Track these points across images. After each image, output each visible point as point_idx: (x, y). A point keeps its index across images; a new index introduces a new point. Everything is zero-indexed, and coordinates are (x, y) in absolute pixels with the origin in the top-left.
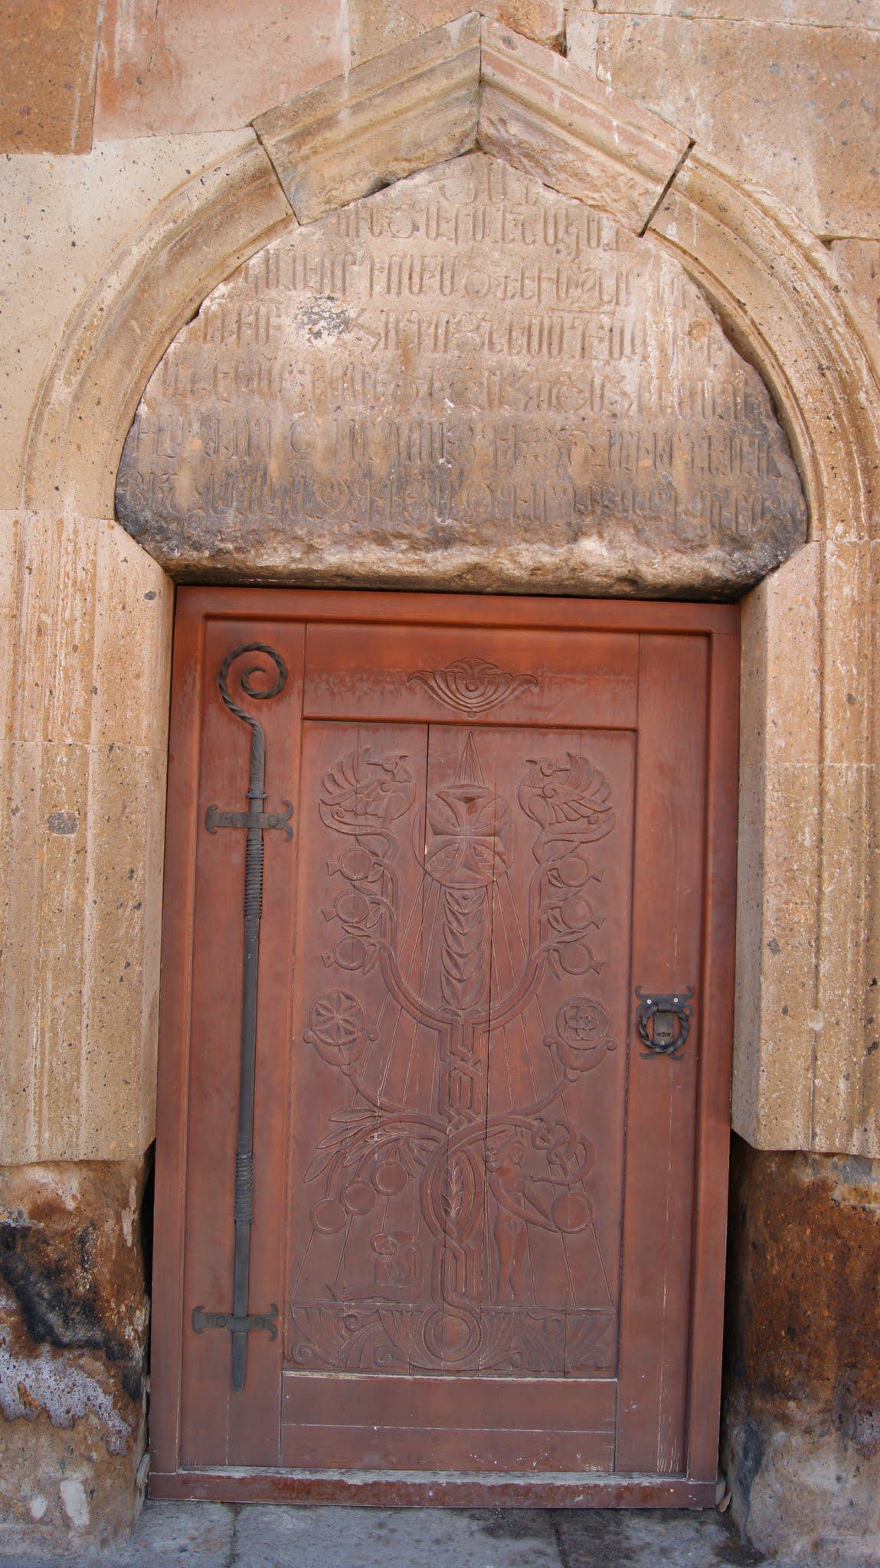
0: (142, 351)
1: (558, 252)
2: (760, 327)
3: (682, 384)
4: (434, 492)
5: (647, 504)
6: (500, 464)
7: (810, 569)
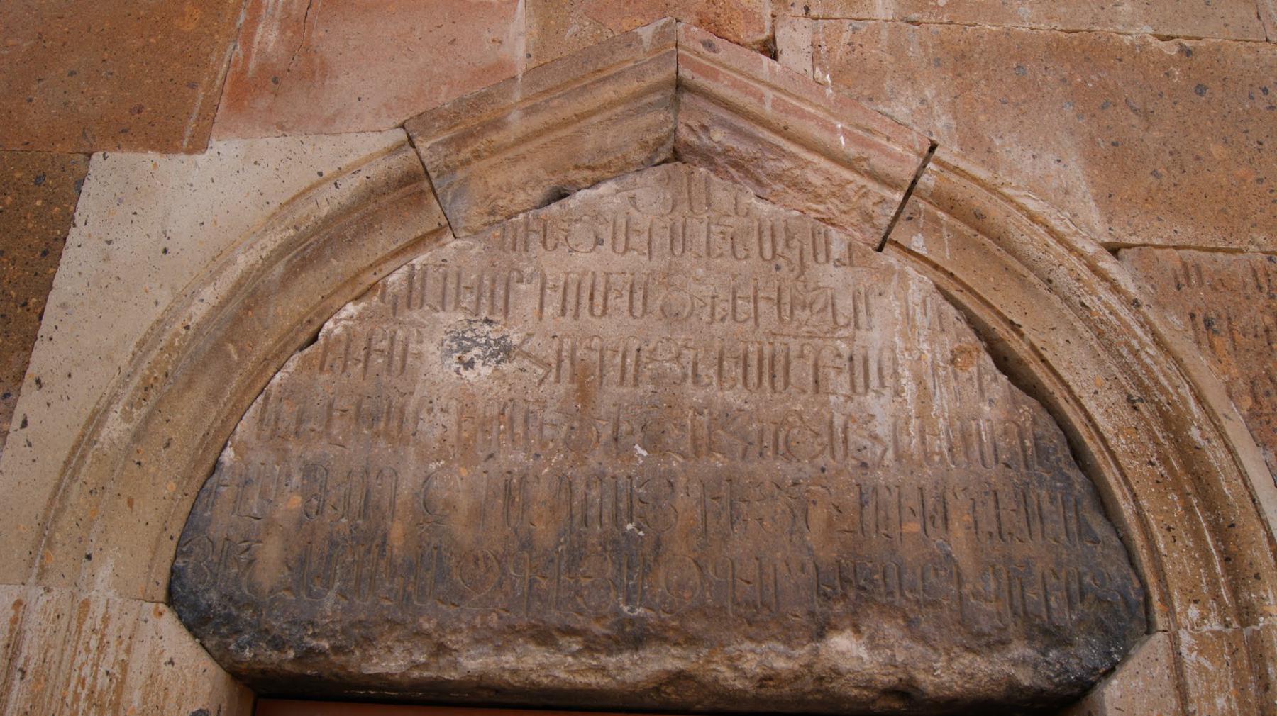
0: (236, 380)
1: (778, 268)
2: (1043, 352)
3: (951, 425)
4: (619, 570)
5: (920, 585)
6: (711, 530)
7: (1161, 671)
